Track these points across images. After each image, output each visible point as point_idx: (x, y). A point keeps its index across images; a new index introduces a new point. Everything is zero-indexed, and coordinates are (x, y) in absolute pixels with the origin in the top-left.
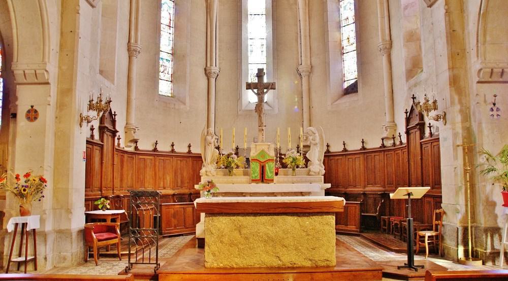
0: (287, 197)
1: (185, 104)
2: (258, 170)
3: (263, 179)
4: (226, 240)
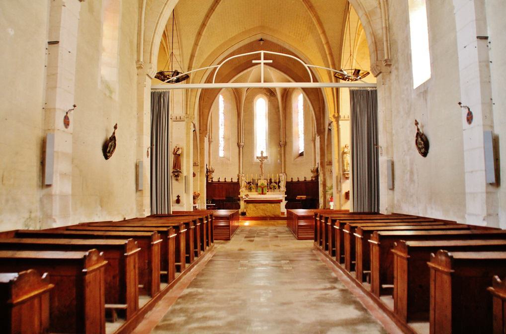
0: (302, 107)
1: (229, 160)
2: (261, 190)
3: (263, 193)
4: (252, 210)
